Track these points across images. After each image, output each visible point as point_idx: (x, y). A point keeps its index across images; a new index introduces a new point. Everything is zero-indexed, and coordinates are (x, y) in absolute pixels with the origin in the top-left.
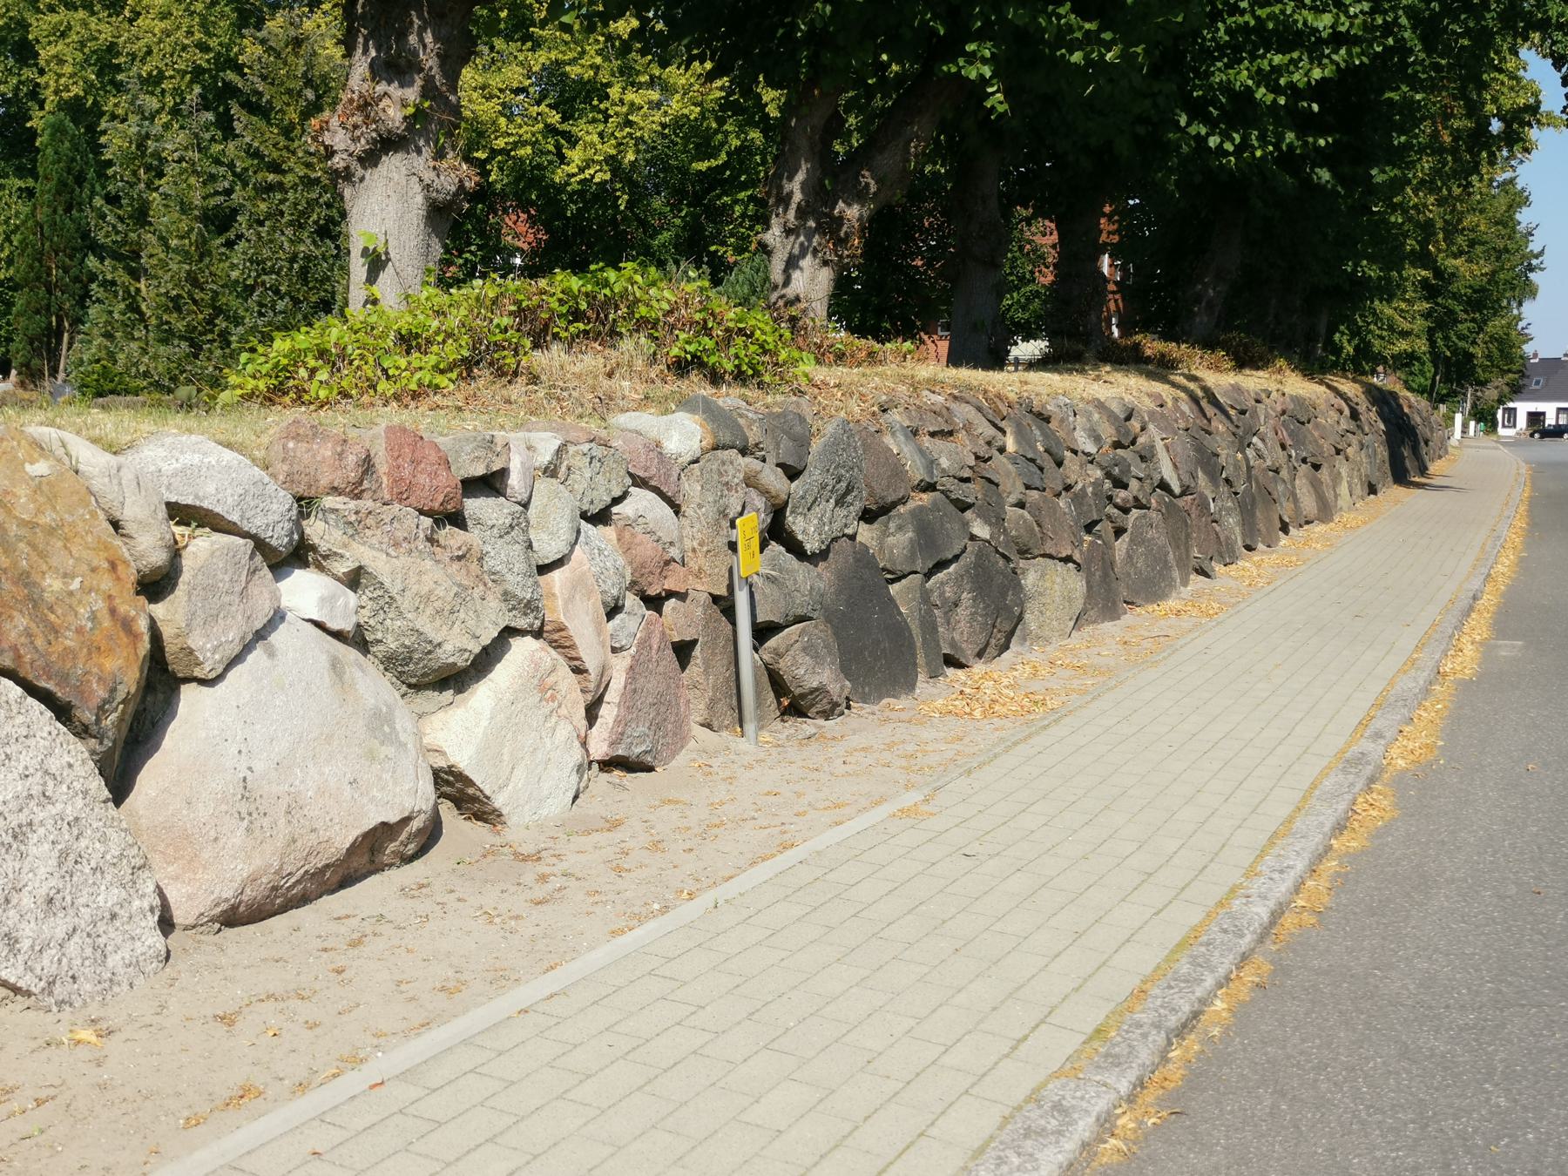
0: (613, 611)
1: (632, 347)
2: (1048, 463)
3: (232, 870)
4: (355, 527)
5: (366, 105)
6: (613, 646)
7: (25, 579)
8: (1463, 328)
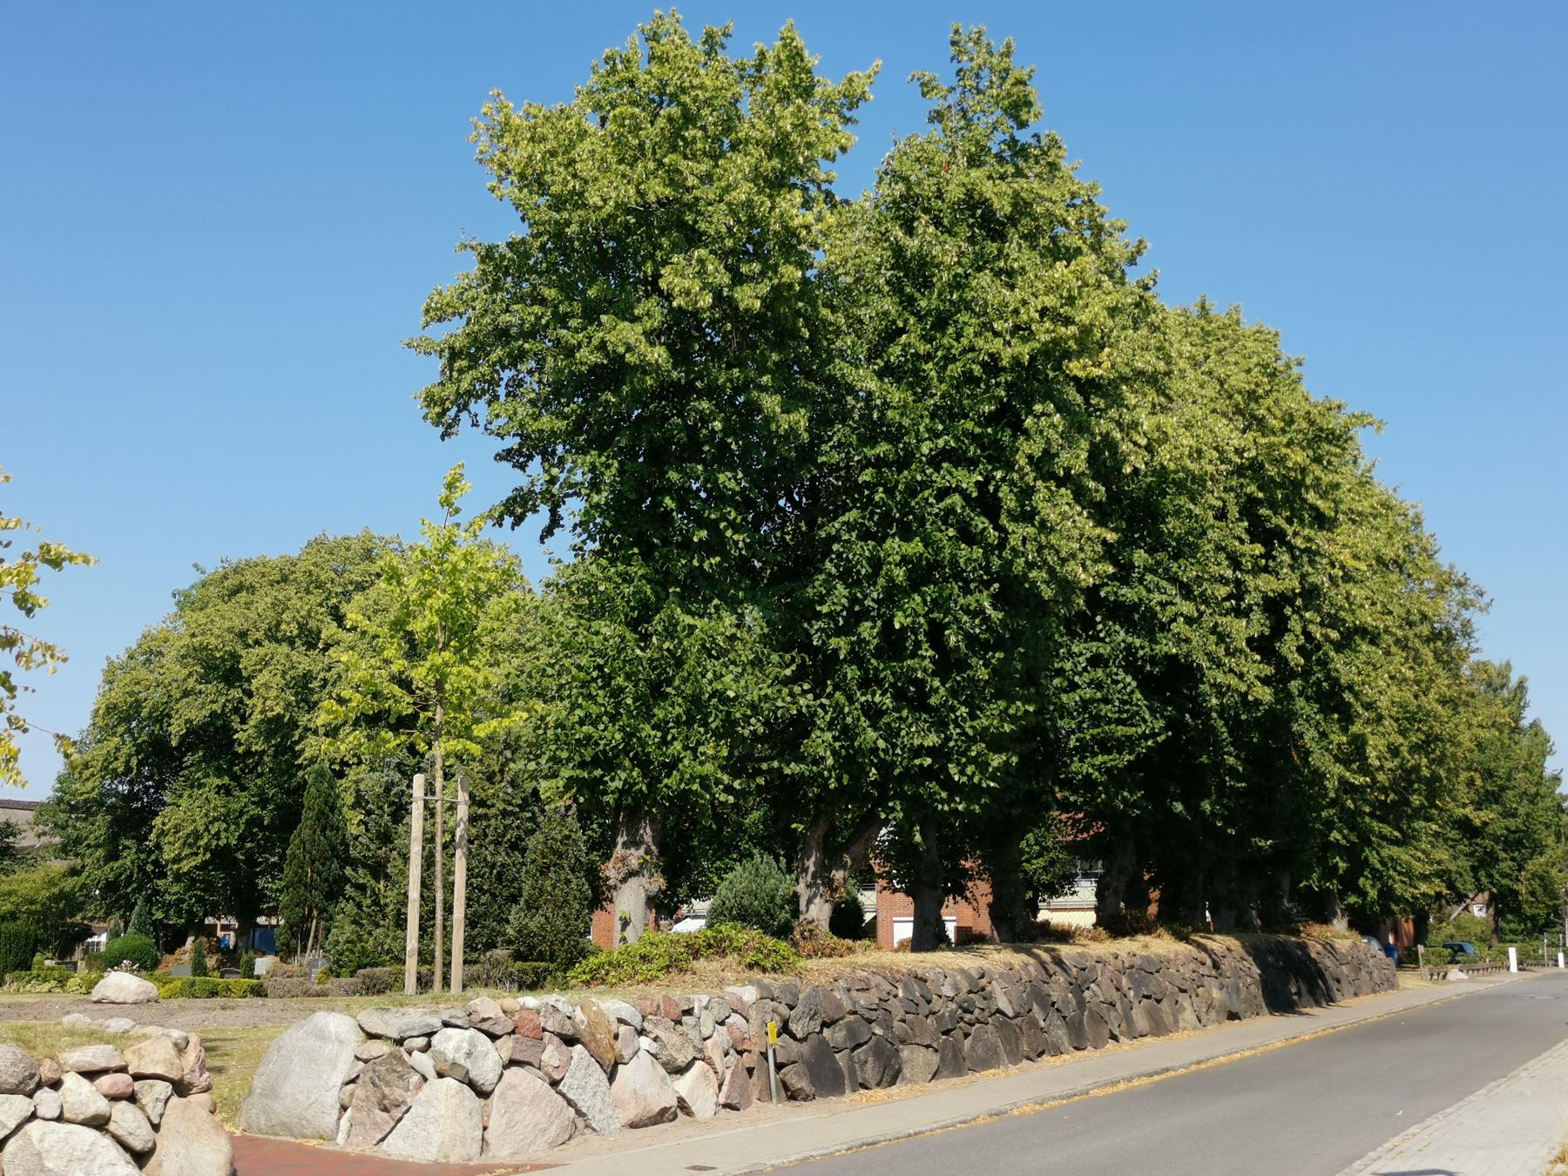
0: (726, 1054)
1: (732, 958)
2: (922, 1002)
3: (632, 1113)
4: (656, 1025)
5: (623, 859)
6: (728, 1066)
8: (1505, 866)
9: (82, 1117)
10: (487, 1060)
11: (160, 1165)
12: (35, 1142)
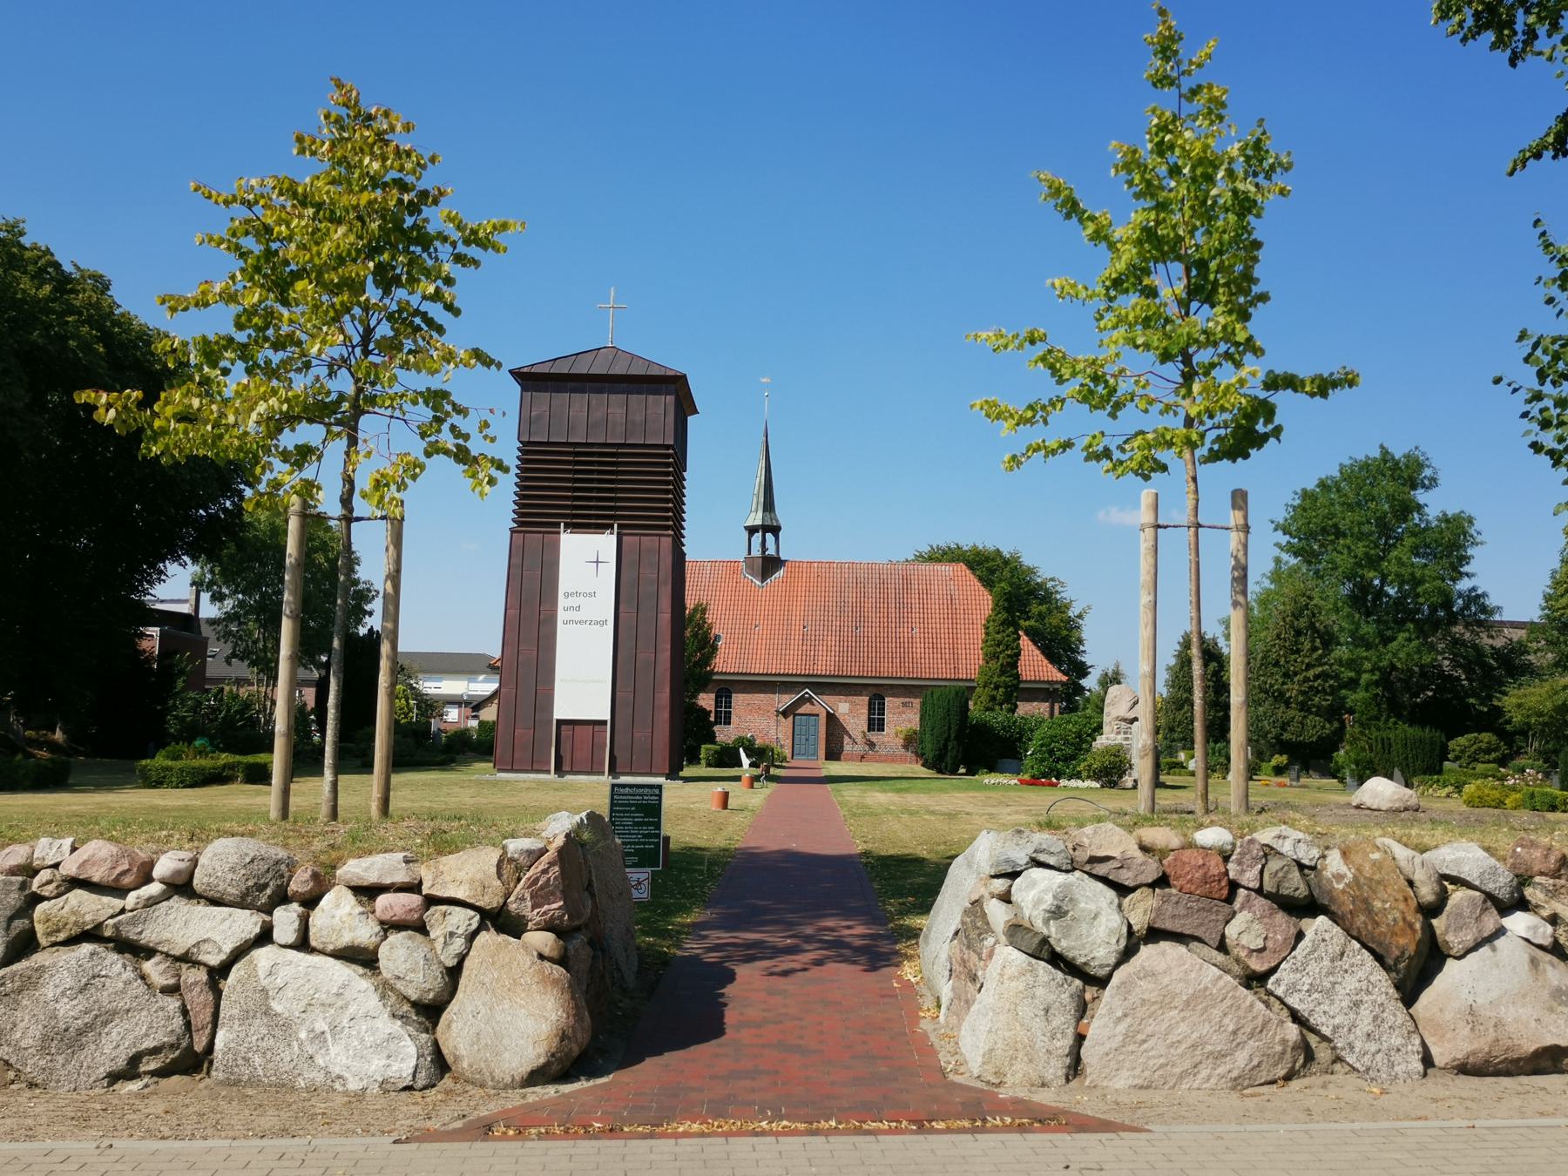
4: (1554, 893)
7: (1366, 901)
9: (330, 947)
10: (1098, 926)
11: (449, 1026)
12: (261, 973)
